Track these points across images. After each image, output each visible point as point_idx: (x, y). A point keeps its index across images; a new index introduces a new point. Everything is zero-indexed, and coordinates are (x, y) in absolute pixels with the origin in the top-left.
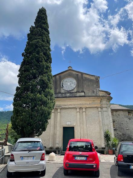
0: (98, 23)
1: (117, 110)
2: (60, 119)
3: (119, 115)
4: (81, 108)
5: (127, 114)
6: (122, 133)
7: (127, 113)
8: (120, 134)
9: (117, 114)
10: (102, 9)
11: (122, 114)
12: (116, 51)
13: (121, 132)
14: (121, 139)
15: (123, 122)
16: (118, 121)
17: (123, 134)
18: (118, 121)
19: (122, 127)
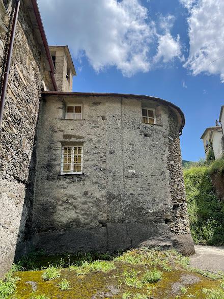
0: (132, 45)
1: (97, 99)
2: (38, 116)
3: (103, 118)
4: (47, 280)
5: (140, 116)
6: (104, 192)
7: (135, 112)
8: (98, 194)
9: (95, 114)
10: (176, 41)
11: (118, 112)
12: (160, 18)
13: (101, 187)
14: (95, 217)
15: (117, 148)
16: (95, 139)
17: (110, 197)
18: (95, 139)
19: (109, 165)
